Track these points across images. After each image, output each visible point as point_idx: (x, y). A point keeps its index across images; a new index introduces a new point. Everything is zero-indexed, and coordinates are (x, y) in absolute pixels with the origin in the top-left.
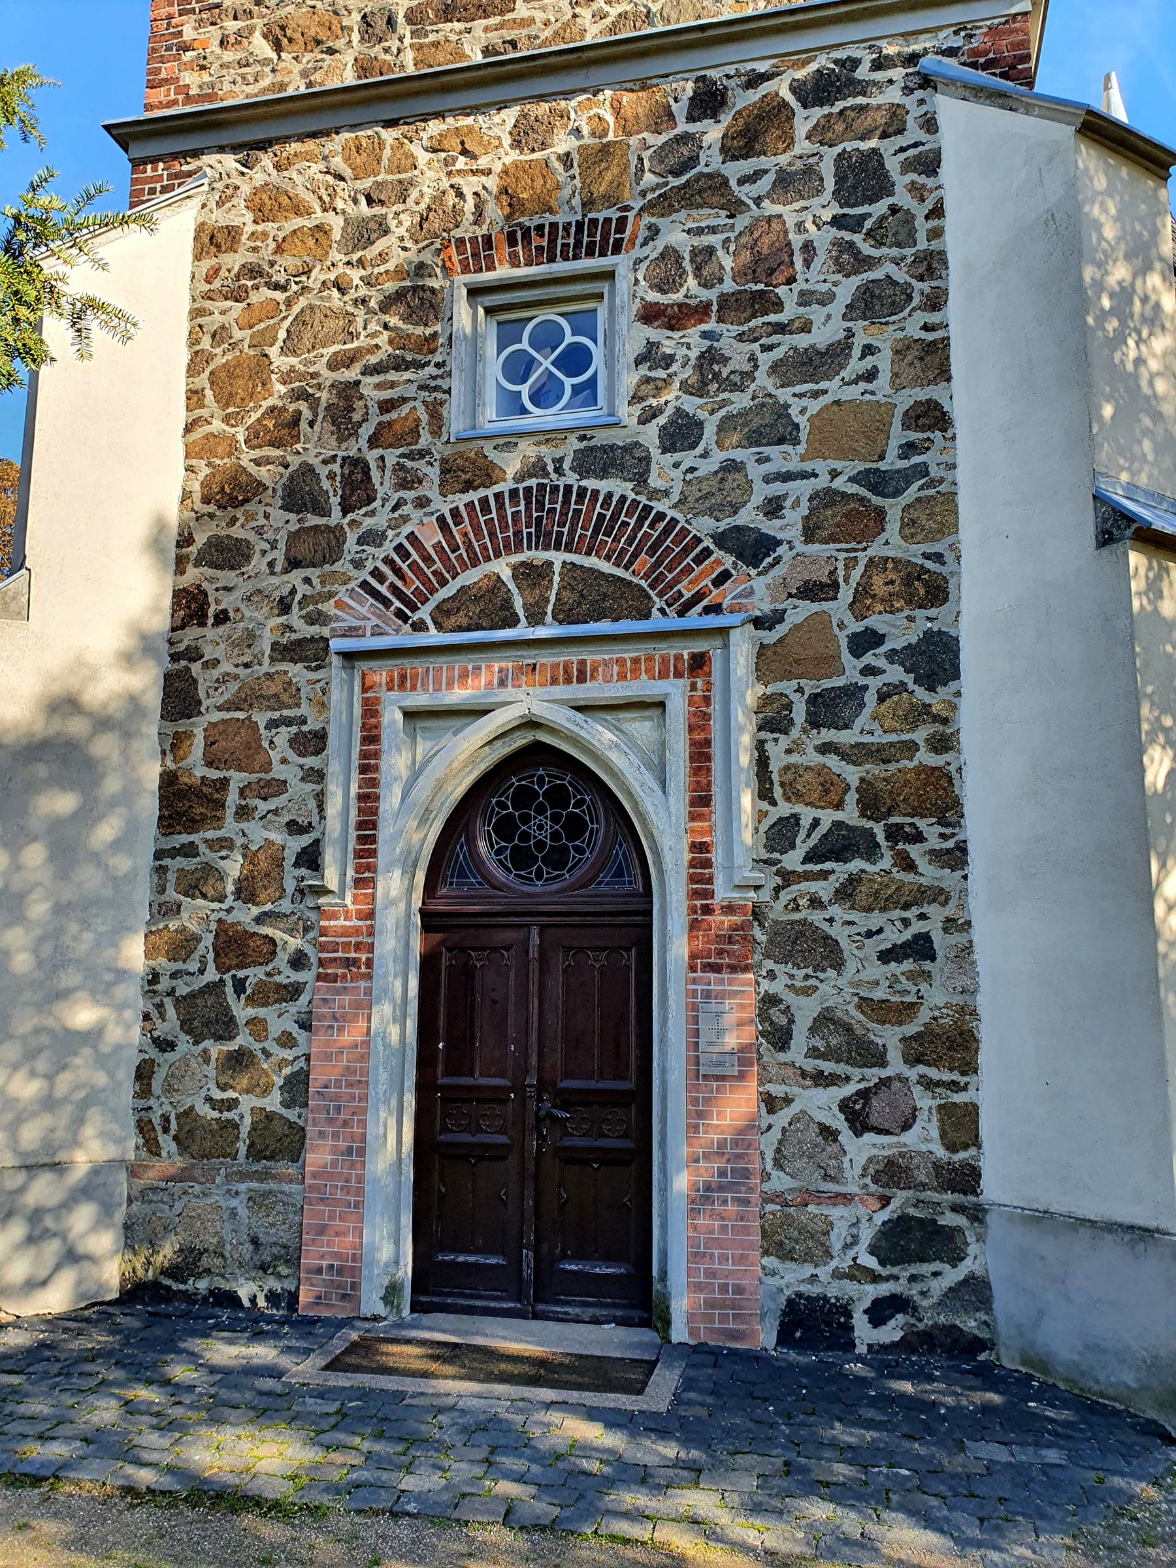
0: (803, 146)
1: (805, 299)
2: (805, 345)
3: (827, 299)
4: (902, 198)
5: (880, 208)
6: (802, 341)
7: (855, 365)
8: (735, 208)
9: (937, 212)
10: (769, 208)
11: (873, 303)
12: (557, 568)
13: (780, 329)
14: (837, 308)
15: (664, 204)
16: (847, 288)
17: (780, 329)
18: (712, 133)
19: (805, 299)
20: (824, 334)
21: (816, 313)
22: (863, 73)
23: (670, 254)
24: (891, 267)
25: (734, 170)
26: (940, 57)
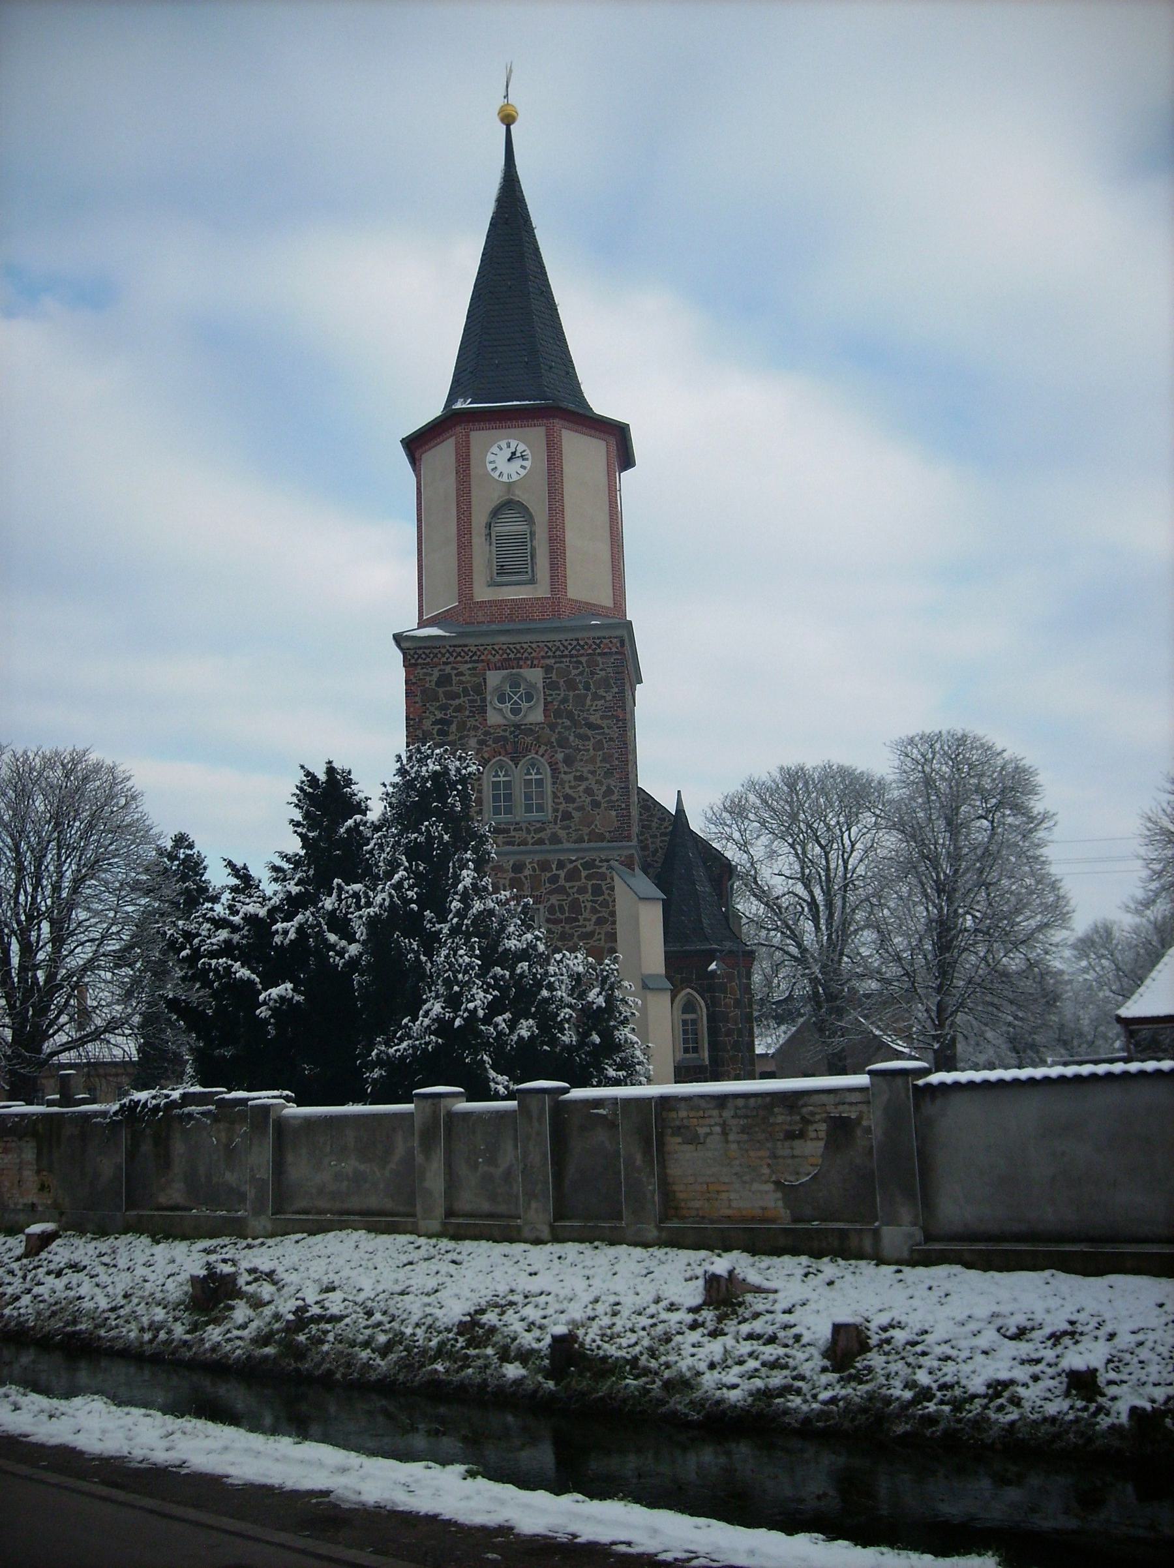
0: (583, 880)
1: (585, 920)
2: (454, 1310)
3: (590, 920)
4: (607, 897)
5: (601, 898)
6: (584, 930)
7: (596, 937)
8: (568, 895)
9: (614, 901)
10: (576, 896)
11: (600, 922)
12: (589, 887)
13: (579, 926)
14: (592, 923)
15: (551, 893)
16: (594, 918)
17: (579, 926)
18: (562, 874)
19: (585, 920)
20: (589, 929)
21: (587, 923)
22: (597, 863)
23: (552, 906)
24: (604, 913)
25: (567, 885)
26: (767, 1285)
